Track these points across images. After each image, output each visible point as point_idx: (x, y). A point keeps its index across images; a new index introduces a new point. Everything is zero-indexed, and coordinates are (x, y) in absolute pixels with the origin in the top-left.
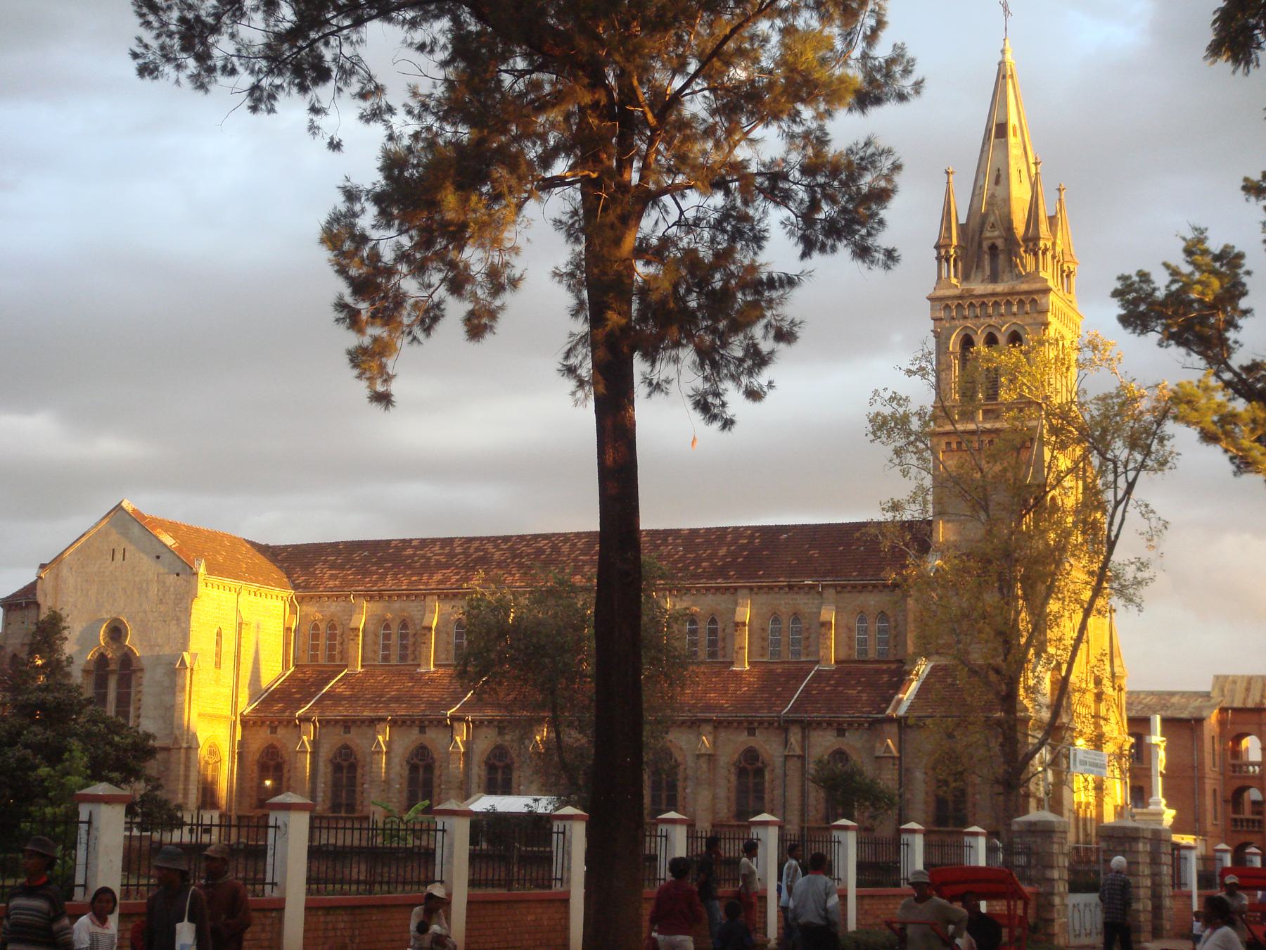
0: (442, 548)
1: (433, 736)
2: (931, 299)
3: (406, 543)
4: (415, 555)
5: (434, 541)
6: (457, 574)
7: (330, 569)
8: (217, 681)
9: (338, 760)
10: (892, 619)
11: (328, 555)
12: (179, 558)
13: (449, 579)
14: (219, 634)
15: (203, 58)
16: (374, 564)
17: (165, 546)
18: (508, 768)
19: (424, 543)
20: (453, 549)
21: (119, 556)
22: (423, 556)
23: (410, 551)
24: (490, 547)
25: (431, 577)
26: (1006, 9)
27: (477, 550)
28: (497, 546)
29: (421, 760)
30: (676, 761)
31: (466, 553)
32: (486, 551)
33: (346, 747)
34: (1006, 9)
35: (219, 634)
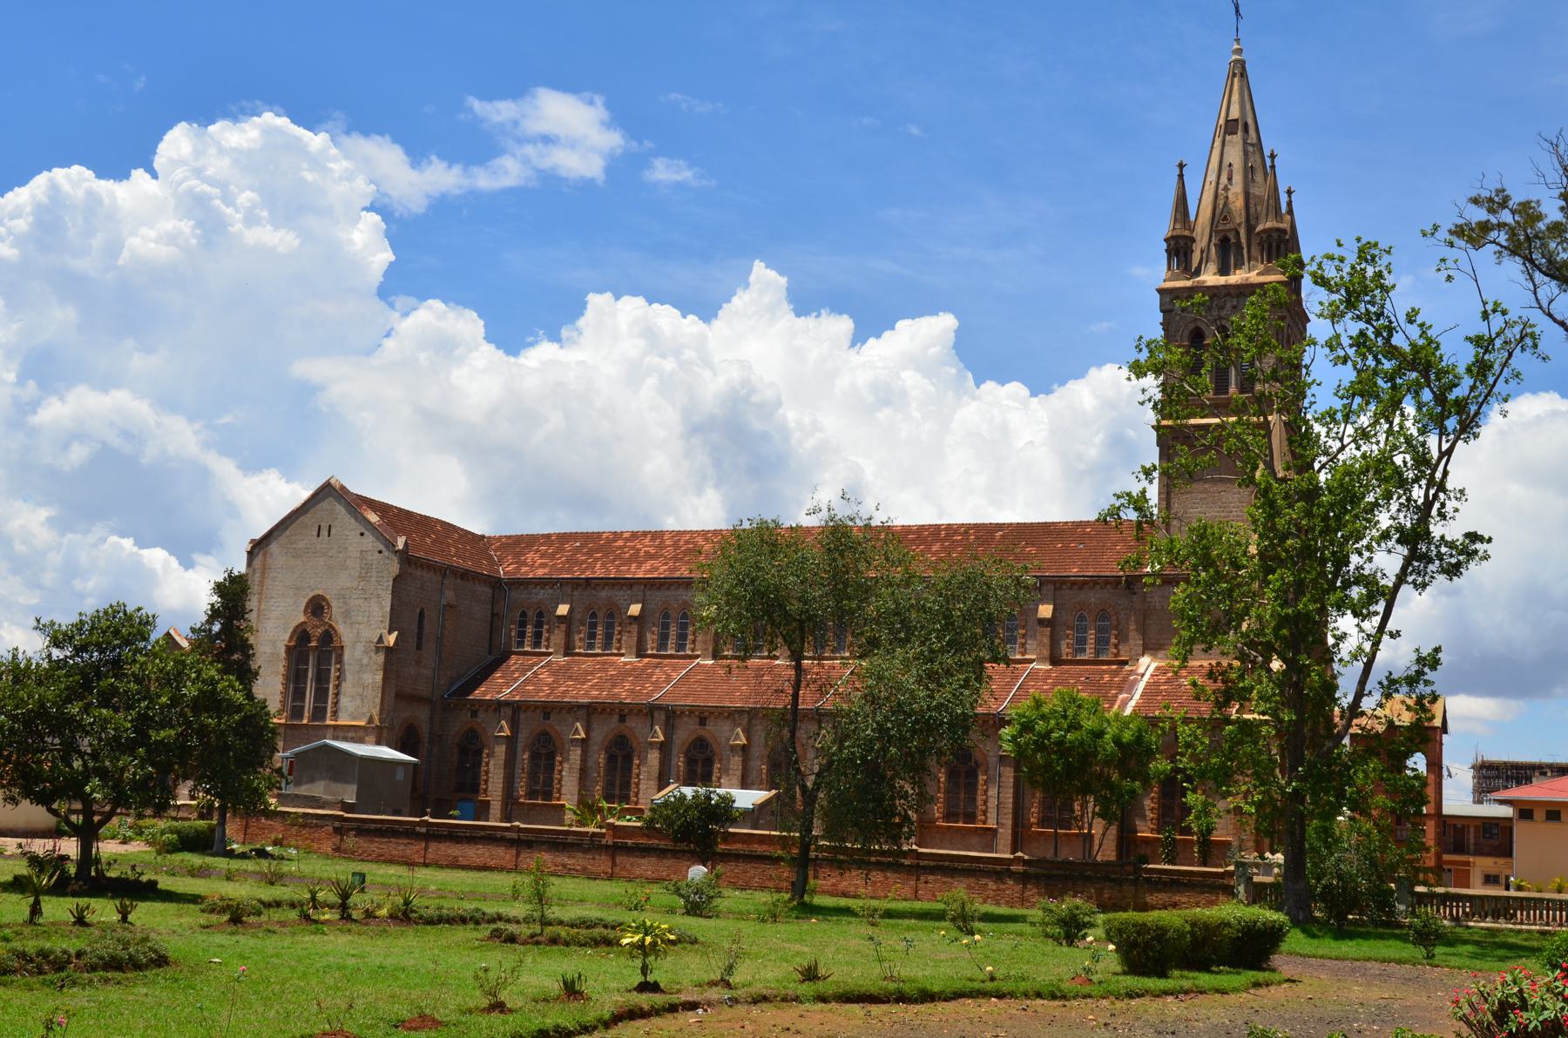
0: (653, 539)
1: (634, 725)
2: (1161, 291)
3: (617, 535)
4: (625, 546)
5: (645, 534)
6: (666, 564)
7: (541, 558)
8: (418, 662)
9: (614, 749)
10: (1114, 618)
11: (542, 545)
12: (382, 535)
13: (657, 568)
14: (421, 615)
15: (799, 888)
16: (584, 554)
17: (369, 522)
18: (709, 762)
19: (634, 535)
20: (663, 542)
21: (324, 532)
22: (633, 548)
23: (620, 543)
24: (700, 541)
25: (639, 567)
26: (1237, 11)
27: (687, 542)
28: (706, 540)
29: (620, 749)
30: (976, 762)
31: (676, 545)
32: (695, 544)
33: (545, 734)
34: (1237, 11)
35: (421, 615)
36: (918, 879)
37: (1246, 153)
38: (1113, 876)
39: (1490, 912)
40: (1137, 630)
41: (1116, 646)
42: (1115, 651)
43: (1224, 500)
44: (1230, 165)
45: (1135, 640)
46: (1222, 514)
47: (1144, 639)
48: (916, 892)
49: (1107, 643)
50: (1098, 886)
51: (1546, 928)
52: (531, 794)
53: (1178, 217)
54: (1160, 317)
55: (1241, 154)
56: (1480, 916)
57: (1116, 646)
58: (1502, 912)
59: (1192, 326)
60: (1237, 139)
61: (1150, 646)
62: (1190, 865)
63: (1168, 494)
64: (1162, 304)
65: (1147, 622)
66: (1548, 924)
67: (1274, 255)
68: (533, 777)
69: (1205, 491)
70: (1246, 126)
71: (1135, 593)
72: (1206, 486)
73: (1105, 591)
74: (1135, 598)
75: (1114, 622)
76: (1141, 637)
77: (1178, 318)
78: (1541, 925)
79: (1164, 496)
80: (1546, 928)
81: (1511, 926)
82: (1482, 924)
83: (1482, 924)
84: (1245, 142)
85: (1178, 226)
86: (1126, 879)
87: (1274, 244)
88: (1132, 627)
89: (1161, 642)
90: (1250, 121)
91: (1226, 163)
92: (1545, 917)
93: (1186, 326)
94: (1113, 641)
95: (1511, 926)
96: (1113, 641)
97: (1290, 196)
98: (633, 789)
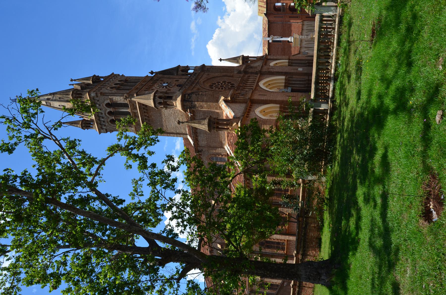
2: (100, 133)
36: (305, 287)
37: (55, 100)
38: (304, 226)
39: (326, 60)
40: (215, 150)
41: (222, 155)
42: (224, 156)
43: (168, 115)
44: (59, 106)
45: (219, 150)
46: (173, 116)
47: (218, 148)
48: (310, 288)
49: (221, 158)
50: (308, 231)
51: (336, 30)
52: (283, 249)
53: (76, 125)
54: (109, 133)
55: (55, 102)
56: (329, 65)
57: (222, 155)
58: (327, 54)
59: (110, 123)
60: (52, 103)
61: (221, 145)
62: (300, 192)
63: (168, 133)
64: (104, 133)
65: (212, 146)
66: (335, 21)
67: (81, 96)
68: (278, 248)
69: (165, 121)
70: (48, 99)
71: (202, 150)
72: (163, 121)
73: (203, 158)
74: (204, 150)
75: (214, 155)
76: (218, 149)
77: (108, 127)
78: (335, 25)
79: (169, 135)
80: (336, 30)
81: (334, 50)
82: (333, 65)
83: (333, 65)
84: (52, 100)
85: (79, 126)
86: (305, 221)
87: (77, 96)
88: (214, 151)
89: (219, 142)
90: (46, 97)
91: (59, 107)
92: (331, 22)
93: (110, 125)
94: (220, 156)
95: (334, 50)
96: (220, 156)
97: (73, 80)
98: (279, 241)
